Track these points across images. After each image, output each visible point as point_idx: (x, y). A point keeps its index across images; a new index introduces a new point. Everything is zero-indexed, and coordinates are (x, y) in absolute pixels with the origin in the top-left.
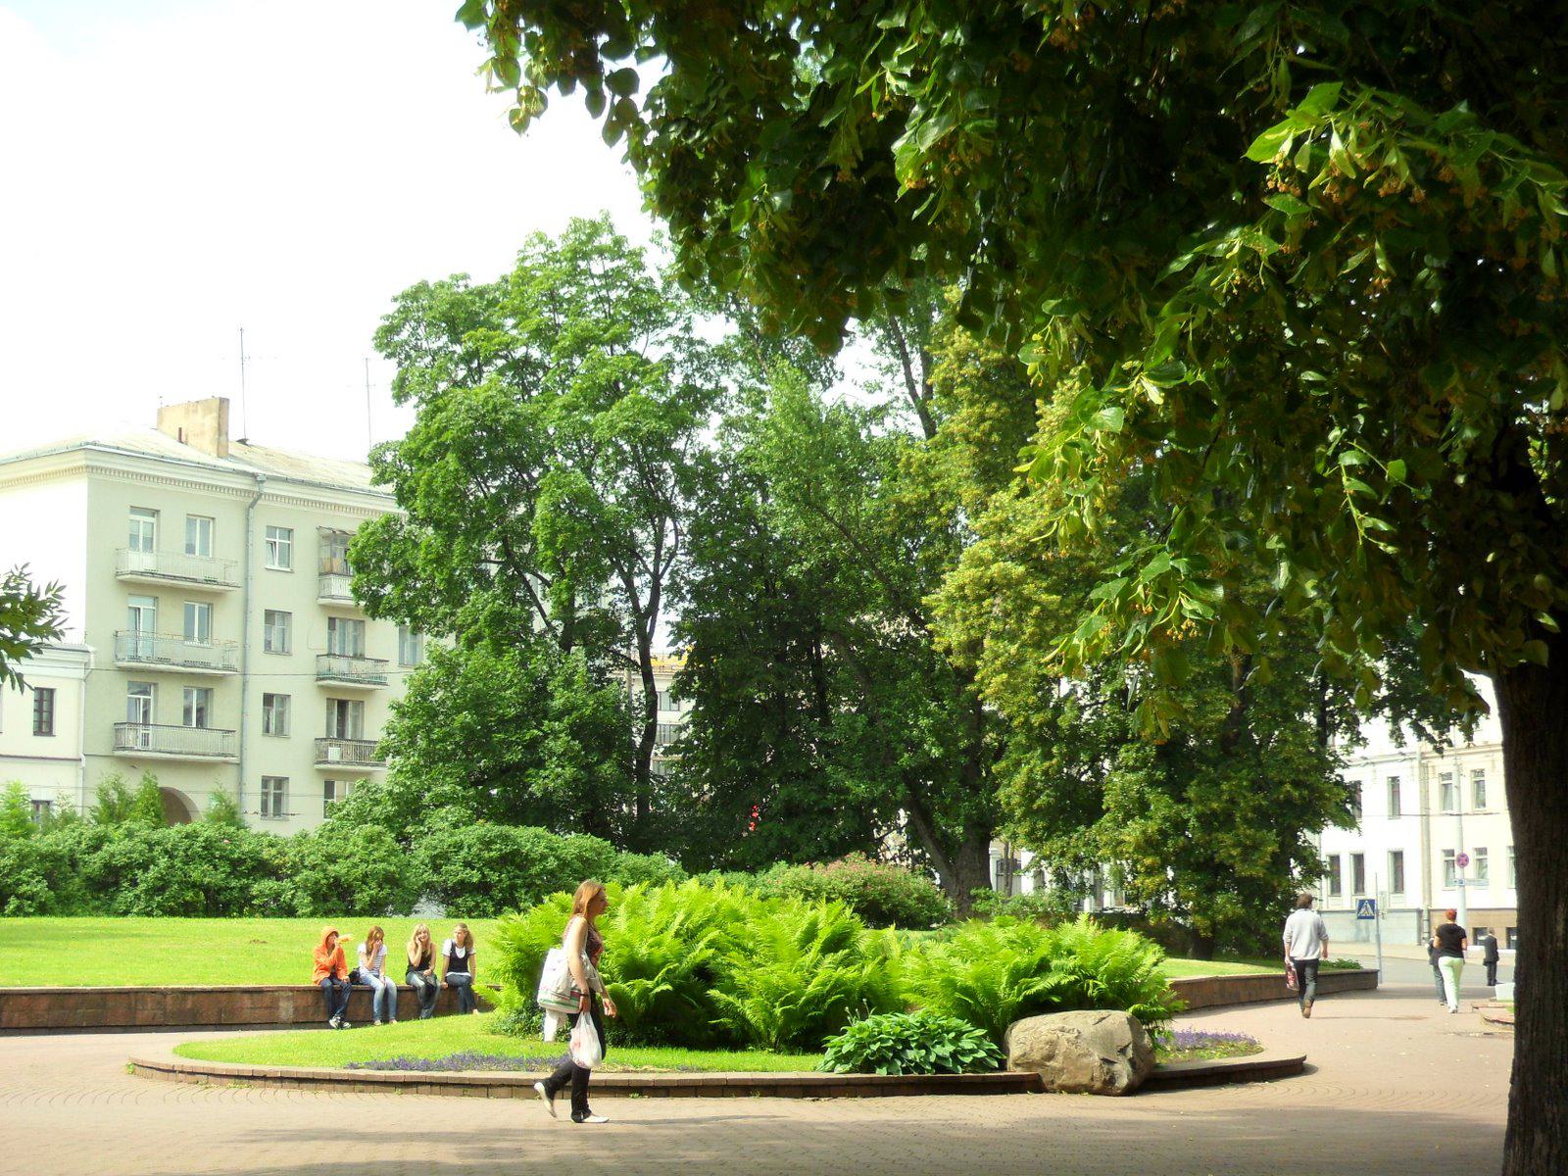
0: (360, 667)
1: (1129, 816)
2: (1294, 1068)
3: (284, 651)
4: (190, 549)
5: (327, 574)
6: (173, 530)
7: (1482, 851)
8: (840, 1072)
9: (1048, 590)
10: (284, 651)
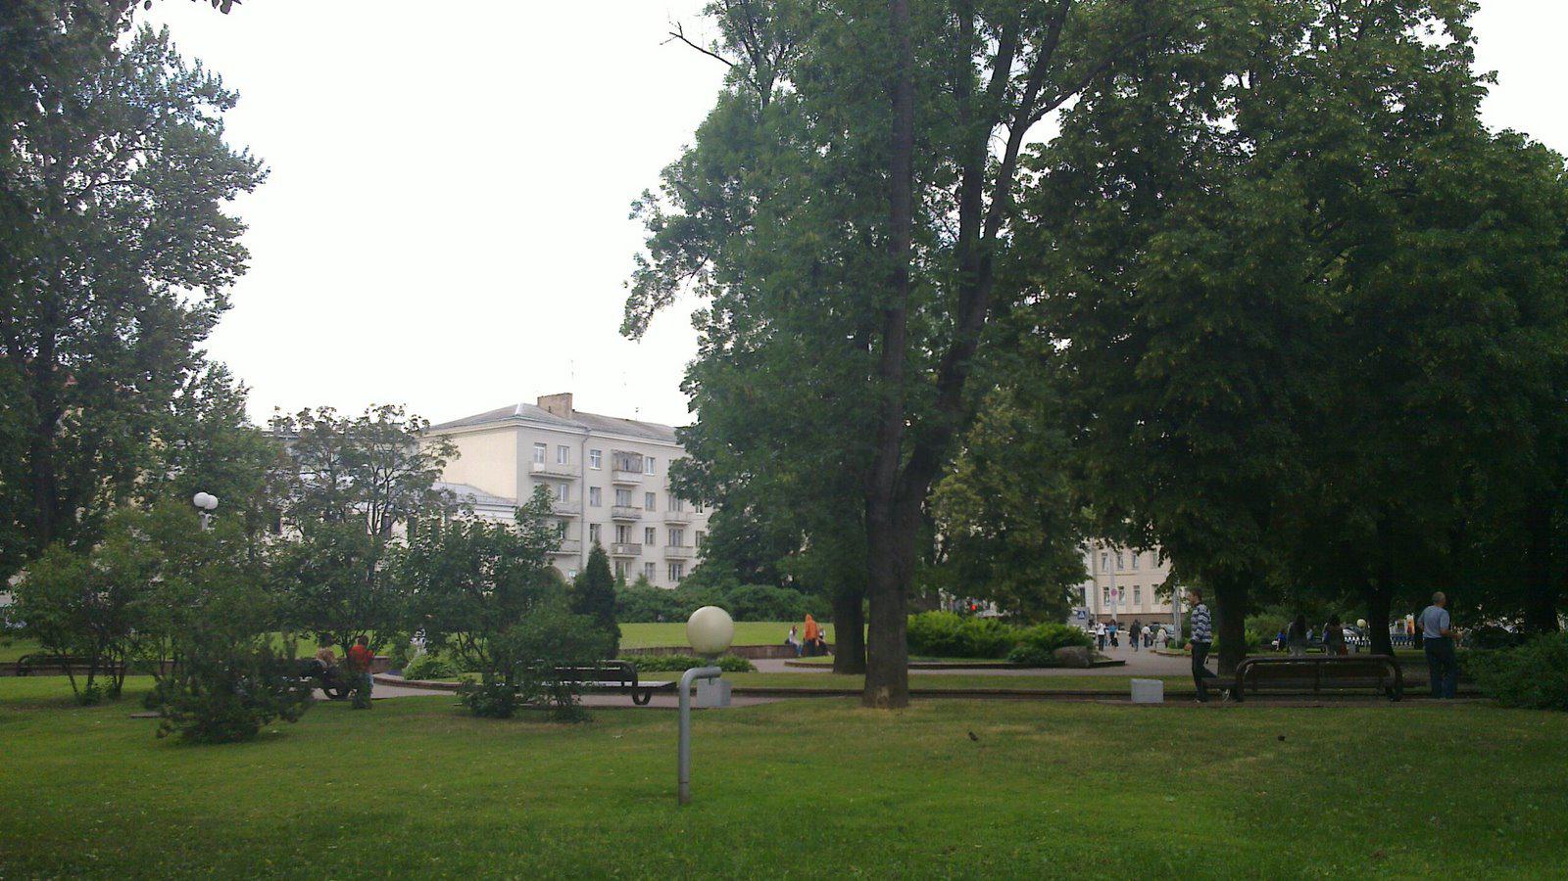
0: (630, 512)
1: (1004, 578)
2: (1121, 663)
3: (599, 505)
4: (559, 461)
5: (617, 470)
6: (552, 452)
7: (1122, 588)
8: (1012, 663)
9: (976, 494)
10: (599, 505)
